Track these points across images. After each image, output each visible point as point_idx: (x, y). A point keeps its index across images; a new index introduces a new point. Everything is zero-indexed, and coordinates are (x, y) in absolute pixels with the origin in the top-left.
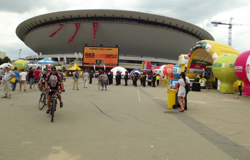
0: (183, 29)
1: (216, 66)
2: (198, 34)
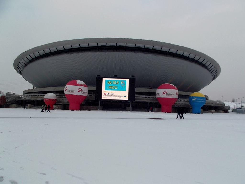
0: (194, 60)
1: (212, 73)
2: (201, 61)
